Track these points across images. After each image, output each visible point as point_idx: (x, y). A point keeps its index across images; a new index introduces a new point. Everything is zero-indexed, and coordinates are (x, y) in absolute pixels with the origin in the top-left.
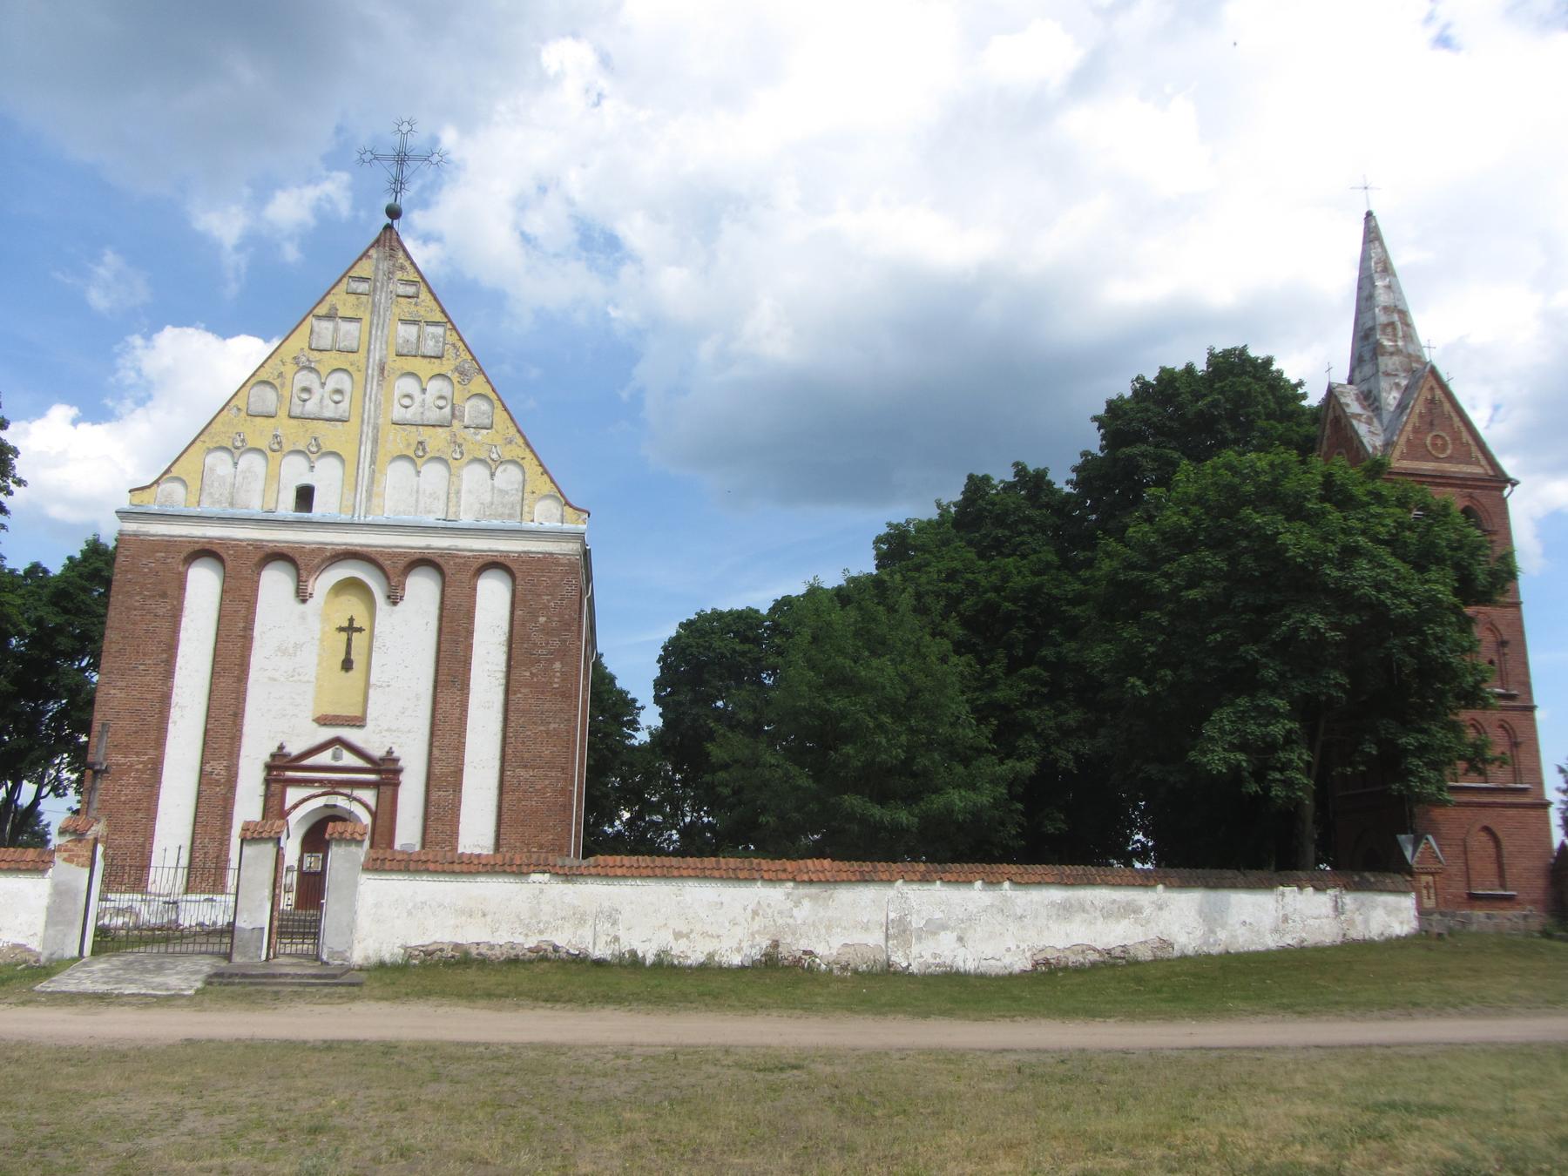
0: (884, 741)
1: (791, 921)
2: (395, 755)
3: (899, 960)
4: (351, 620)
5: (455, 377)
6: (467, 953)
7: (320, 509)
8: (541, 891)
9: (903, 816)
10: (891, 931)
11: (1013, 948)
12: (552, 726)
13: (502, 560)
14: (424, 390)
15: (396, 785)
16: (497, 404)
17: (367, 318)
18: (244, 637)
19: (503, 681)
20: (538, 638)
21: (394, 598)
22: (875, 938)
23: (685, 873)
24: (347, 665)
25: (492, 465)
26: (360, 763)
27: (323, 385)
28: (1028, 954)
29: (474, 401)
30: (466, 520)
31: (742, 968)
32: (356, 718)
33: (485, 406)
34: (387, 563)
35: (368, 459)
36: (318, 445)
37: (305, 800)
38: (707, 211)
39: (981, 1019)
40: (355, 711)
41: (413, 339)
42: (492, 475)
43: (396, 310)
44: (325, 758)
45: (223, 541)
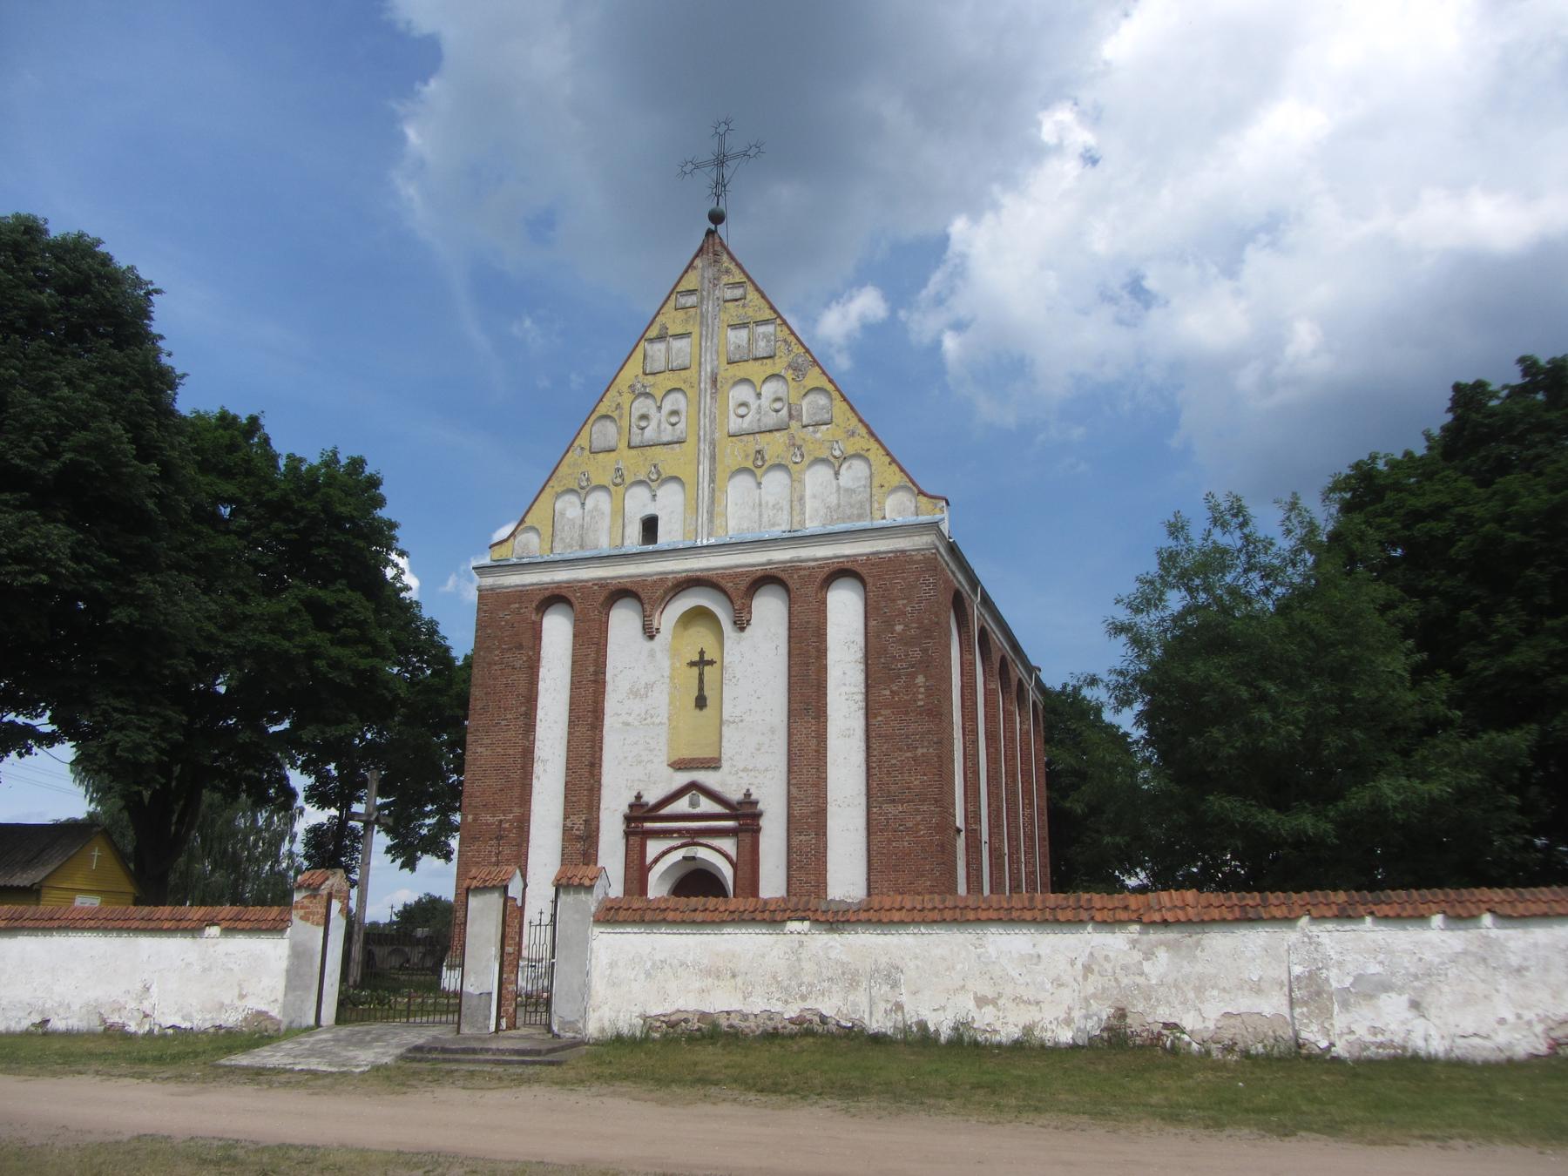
0: (1267, 716)
1: (1141, 980)
2: (753, 797)
3: (1314, 1036)
4: (702, 653)
5: (789, 375)
6: (715, 1025)
7: (665, 538)
8: (801, 944)
9: (1306, 822)
10: (1297, 994)
11: (1511, 1018)
12: (920, 751)
13: (848, 566)
14: (759, 395)
15: (756, 831)
16: (835, 395)
17: (696, 331)
18: (595, 681)
19: (863, 704)
20: (895, 650)
21: (741, 624)
22: (1273, 1005)
23: (983, 915)
24: (701, 702)
25: (835, 463)
26: (717, 809)
27: (659, 408)
28: (1539, 1028)
29: (811, 397)
30: (812, 526)
31: (1074, 1048)
32: (713, 760)
33: (822, 400)
34: (729, 586)
35: (707, 479)
36: (658, 473)
37: (665, 853)
38: (1230, 243)
39: (1384, 1142)
40: (707, 753)
41: (744, 343)
42: (837, 474)
43: (723, 316)
44: (682, 806)
45: (570, 585)
